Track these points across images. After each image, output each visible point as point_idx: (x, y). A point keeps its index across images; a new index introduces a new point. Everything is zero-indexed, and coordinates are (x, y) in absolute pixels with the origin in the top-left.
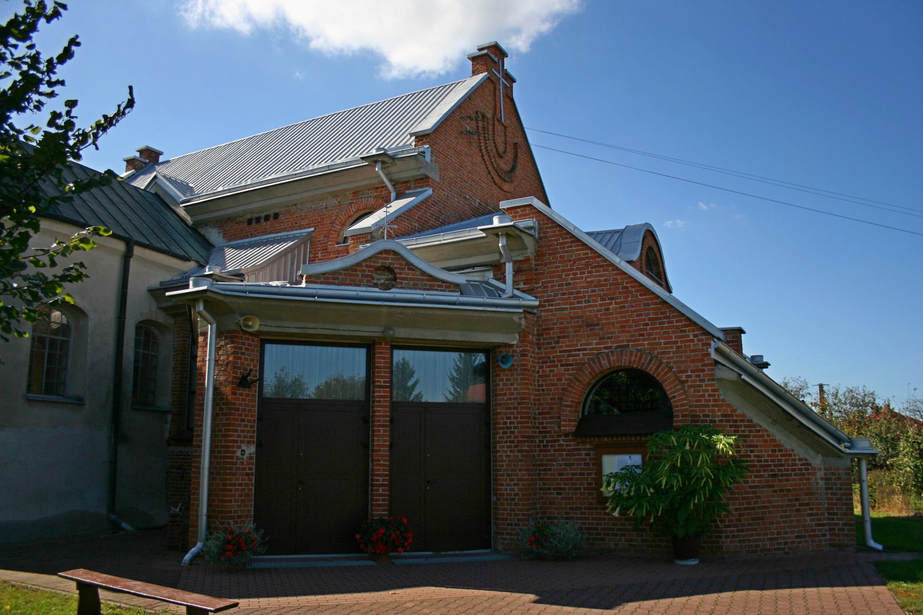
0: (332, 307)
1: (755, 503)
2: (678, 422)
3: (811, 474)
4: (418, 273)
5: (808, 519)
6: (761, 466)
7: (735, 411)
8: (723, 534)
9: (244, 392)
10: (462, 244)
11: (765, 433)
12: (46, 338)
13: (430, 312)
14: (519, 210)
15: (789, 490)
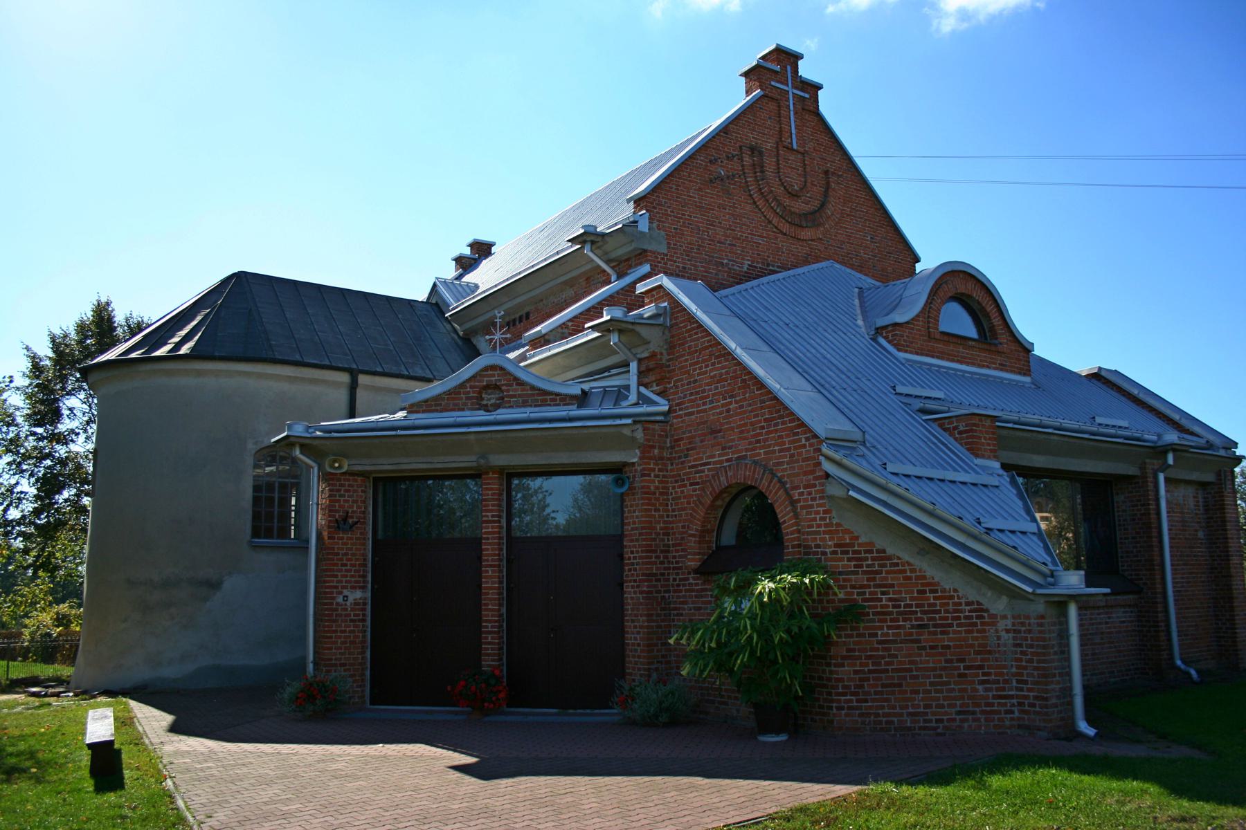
0: (356, 441)
1: (887, 664)
2: (788, 554)
3: (988, 624)
4: (528, 387)
5: (980, 688)
6: (899, 613)
7: (857, 538)
8: (834, 705)
9: (345, 536)
10: (591, 344)
11: (907, 568)
12: (274, 482)
13: (522, 434)
14: (654, 293)
15: (948, 647)
